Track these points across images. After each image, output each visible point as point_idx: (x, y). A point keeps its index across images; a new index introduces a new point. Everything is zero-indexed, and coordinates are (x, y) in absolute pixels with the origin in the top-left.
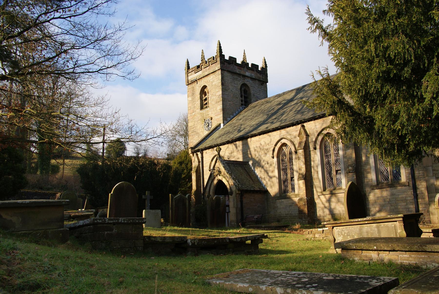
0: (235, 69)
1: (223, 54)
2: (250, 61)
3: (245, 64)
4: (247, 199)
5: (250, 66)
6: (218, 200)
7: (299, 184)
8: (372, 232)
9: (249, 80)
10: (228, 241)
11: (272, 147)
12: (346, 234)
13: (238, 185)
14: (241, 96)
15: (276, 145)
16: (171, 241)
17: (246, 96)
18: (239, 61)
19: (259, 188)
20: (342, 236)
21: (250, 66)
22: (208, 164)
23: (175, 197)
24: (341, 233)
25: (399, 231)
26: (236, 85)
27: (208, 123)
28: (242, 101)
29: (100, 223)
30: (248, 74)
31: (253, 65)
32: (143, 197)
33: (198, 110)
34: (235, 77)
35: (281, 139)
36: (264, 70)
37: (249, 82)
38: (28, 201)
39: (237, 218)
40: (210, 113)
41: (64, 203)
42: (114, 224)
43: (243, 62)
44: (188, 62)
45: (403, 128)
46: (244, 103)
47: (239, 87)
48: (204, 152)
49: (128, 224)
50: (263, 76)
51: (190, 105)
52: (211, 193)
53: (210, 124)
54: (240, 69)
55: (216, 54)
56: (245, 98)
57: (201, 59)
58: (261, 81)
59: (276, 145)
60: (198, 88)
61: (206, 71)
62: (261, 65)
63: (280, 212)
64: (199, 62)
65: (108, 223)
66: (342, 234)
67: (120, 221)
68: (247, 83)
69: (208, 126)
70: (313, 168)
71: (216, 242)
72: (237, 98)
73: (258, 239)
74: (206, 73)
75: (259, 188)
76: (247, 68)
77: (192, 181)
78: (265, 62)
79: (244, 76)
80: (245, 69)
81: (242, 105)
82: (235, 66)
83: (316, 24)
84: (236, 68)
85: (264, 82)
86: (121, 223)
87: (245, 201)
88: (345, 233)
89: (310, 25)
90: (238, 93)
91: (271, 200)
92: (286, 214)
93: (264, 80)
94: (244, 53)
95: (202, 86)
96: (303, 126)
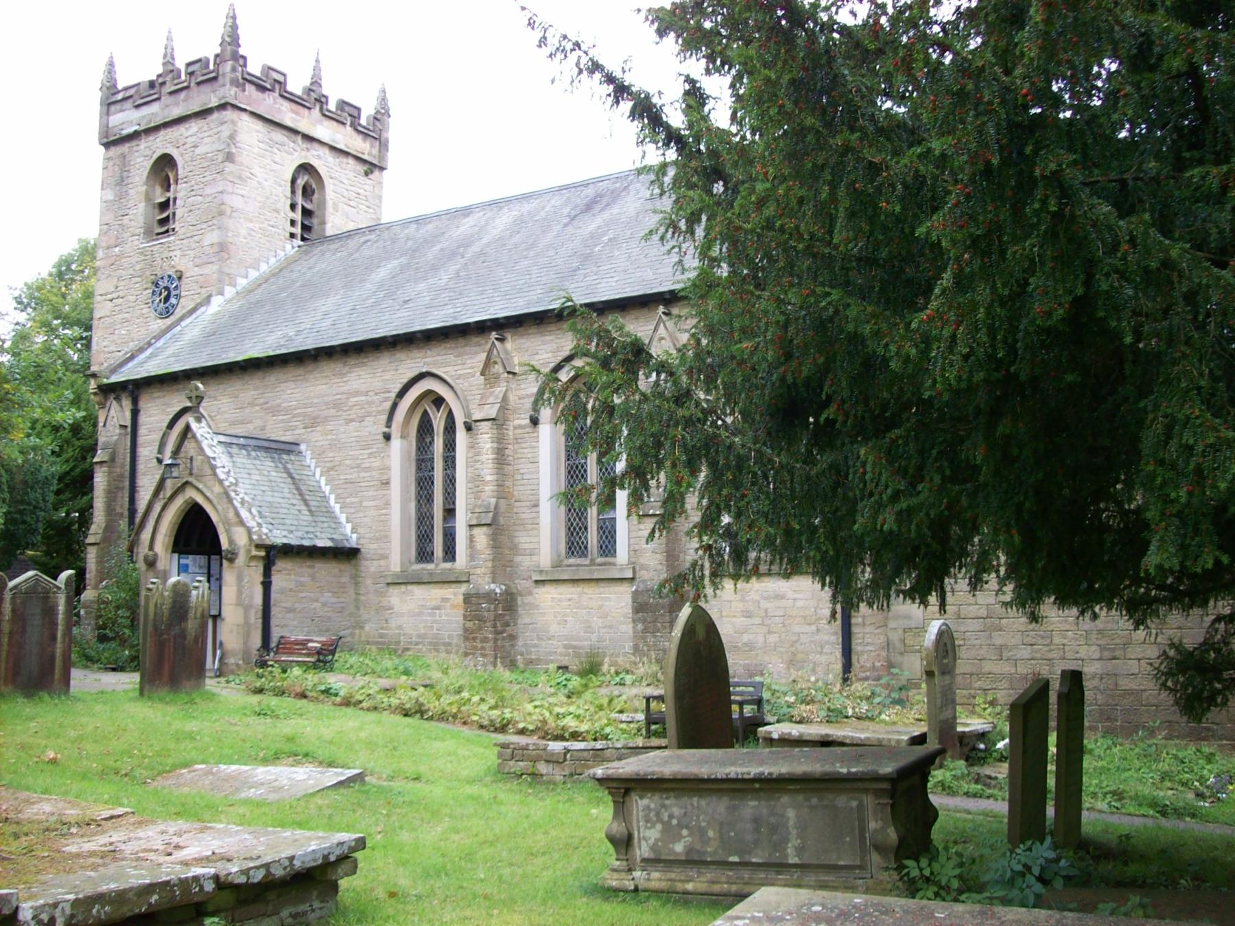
0: (279, 111)
1: (668, 7)
2: (334, 93)
3: (313, 99)
4: (286, 576)
5: (332, 106)
8: (773, 820)
9: (325, 152)
10: (209, 887)
11: (386, 400)
12: (675, 822)
13: (259, 525)
14: (293, 207)
17: (308, 206)
18: (296, 86)
19: (332, 539)
20: (659, 826)
21: (332, 106)
22: (157, 437)
23: (11, 584)
24: (658, 814)
25: (872, 825)
26: (275, 167)
27: (167, 288)
28: (293, 223)
30: (325, 131)
31: (343, 104)
33: (136, 243)
34: (279, 136)
36: (381, 117)
37: (322, 161)
39: (245, 643)
40: (178, 253)
43: (309, 90)
44: (111, 64)
46: (298, 230)
47: (289, 177)
50: (372, 146)
51: (110, 217)
52: (160, 547)
53: (173, 293)
54: (297, 113)
55: (218, 50)
56: (307, 213)
57: (162, 61)
58: (365, 162)
60: (144, 155)
61: (177, 104)
62: (367, 111)
63: (400, 627)
64: (152, 70)
66: (660, 820)
69: (167, 299)
70: (342, 246)
71: (154, 898)
72: (277, 211)
73: (343, 858)
74: (177, 112)
75: (332, 539)
76: (321, 109)
77: (92, 489)
78: (234, 27)
79: (309, 138)
80: (316, 112)
81: (292, 236)
82: (281, 100)
84: (286, 105)
85: (375, 166)
87: (278, 581)
88: (671, 817)
90: (282, 194)
91: (369, 582)
92: (419, 636)
93: (375, 162)
94: (317, 61)
95: (155, 156)
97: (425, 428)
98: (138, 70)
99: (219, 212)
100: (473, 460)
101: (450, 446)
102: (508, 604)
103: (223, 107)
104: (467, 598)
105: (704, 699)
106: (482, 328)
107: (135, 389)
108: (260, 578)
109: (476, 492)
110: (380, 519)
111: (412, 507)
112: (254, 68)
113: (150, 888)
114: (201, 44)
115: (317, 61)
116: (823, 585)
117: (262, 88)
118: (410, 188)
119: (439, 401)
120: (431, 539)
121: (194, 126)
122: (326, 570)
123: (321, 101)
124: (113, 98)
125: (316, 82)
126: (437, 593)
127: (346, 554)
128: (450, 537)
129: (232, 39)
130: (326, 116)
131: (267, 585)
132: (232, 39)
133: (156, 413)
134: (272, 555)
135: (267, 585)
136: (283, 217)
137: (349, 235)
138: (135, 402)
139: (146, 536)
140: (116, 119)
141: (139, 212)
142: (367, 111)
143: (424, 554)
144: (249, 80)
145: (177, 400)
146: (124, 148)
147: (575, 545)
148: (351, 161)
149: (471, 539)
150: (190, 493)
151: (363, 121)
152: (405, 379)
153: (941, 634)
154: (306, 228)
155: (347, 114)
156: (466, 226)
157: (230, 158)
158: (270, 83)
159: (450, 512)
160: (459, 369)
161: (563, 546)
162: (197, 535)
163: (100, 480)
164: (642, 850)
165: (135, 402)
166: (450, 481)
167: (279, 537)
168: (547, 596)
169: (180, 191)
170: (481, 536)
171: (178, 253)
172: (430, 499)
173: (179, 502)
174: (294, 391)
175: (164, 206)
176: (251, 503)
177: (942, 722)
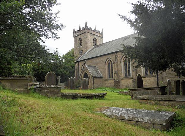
2: (97, 30)
3: (95, 31)
4: (95, 80)
5: (97, 31)
6: (85, 81)
7: (115, 75)
15: (106, 60)
16: (72, 94)
18: (93, 29)
21: (97, 31)
29: (44, 87)
30: (96, 34)
31: (98, 31)
32: (58, 78)
34: (92, 35)
35: (108, 58)
36: (102, 32)
37: (96, 37)
38: (181, 86)
41: (28, 78)
42: (49, 87)
43: (94, 30)
44: (74, 29)
45: (150, 8)
48: (80, 63)
49: (55, 87)
59: (106, 60)
60: (78, 38)
64: (78, 29)
65: (46, 87)
67: (51, 86)
68: (96, 38)
74: (81, 33)
78: (87, 24)
79: (95, 35)
83: (124, 18)
84: (92, 32)
86: (52, 87)
89: (122, 19)
94: (95, 27)
96: (158, 86)
97: (109, 64)
98: (77, 29)
99: (86, 43)
100: (114, 67)
101: (112, 65)
102: (119, 82)
103: (86, 32)
104: (114, 81)
105: (139, 81)
106: (115, 53)
107: (79, 62)
108: (92, 80)
109: (115, 70)
110: (106, 74)
111: (108, 72)
112: (89, 28)
113: (88, 94)
114: (83, 26)
115: (95, 27)
116: (134, 14)
117: (90, 30)
118: (105, 40)
119: (110, 61)
120: (110, 76)
121: (83, 34)
122: (99, 79)
123: (96, 31)
124: (74, 32)
125: (95, 29)
126: (112, 81)
127: (101, 77)
128: (112, 75)
129: (86, 25)
130: (97, 32)
131: (93, 81)
132: (86, 25)
133: (81, 64)
134: (94, 78)
135: (93, 81)
136: (93, 44)
137: (99, 45)
138: (79, 63)
139: (81, 76)
140: (75, 35)
141: (78, 44)
142: (101, 31)
143: (110, 77)
144: (88, 29)
145: (83, 62)
146: (76, 38)
147: (126, 75)
148: (100, 37)
149: (115, 75)
150: (85, 72)
151: (100, 33)
152: (107, 58)
153: (168, 81)
154: (95, 44)
155: (99, 32)
156: (113, 43)
157: (87, 38)
158: (91, 29)
159: (112, 73)
160: (113, 57)
161: (125, 76)
162: (86, 76)
163: (75, 71)
164: (134, 97)
165: (79, 63)
166: (112, 69)
167: (94, 76)
168: (123, 81)
169: (82, 41)
170: (116, 74)
171: (82, 48)
172: (110, 71)
173: (84, 73)
174: (95, 61)
175: (80, 43)
176: (92, 72)
177: (169, 91)
